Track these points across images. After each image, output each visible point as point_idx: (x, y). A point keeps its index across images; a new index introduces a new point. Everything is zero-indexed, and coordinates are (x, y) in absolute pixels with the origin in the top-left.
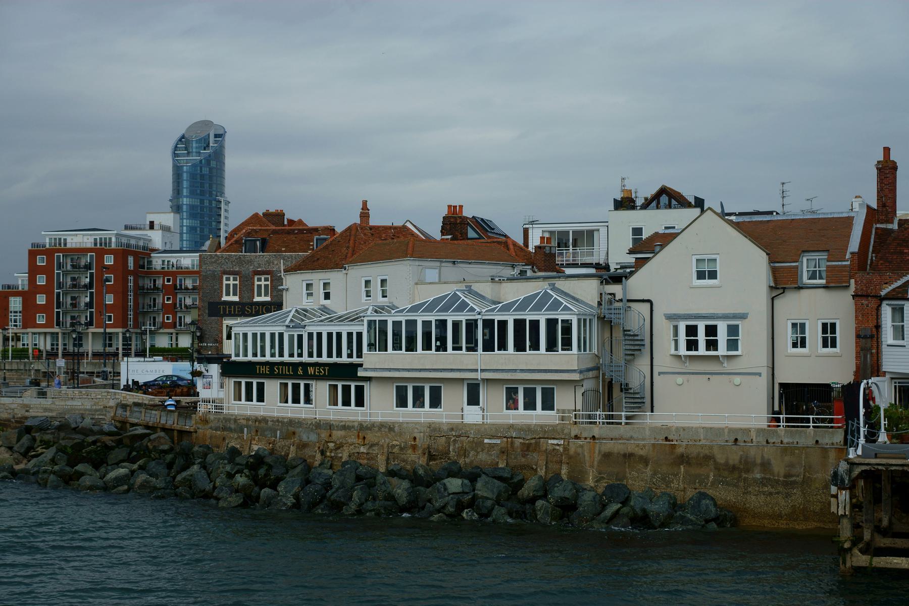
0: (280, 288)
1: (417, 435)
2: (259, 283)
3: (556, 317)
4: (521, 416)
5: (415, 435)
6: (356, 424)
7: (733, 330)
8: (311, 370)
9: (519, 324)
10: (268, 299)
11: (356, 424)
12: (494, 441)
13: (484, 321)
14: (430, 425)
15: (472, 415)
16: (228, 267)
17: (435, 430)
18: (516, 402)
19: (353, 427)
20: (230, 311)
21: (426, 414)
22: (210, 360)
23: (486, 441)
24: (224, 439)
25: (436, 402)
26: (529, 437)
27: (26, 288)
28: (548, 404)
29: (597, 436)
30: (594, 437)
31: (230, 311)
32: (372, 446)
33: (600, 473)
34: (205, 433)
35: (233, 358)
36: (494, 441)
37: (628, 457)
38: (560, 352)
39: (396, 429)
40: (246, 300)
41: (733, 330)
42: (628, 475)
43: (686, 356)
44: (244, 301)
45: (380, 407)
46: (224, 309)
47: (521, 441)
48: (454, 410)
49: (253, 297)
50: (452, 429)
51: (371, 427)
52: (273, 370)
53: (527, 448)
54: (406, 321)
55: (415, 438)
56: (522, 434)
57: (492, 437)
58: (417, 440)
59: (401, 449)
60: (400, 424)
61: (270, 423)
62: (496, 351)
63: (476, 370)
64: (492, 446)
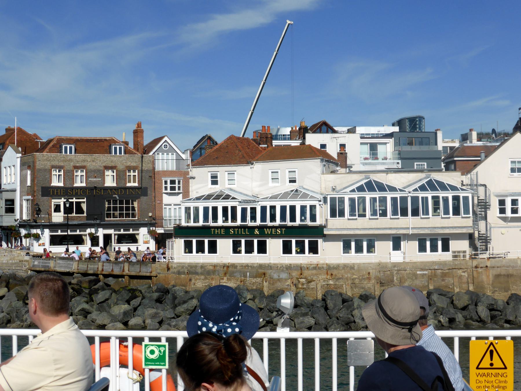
0: (188, 176)
1: (371, 271)
2: (134, 174)
3: (459, 194)
4: (429, 256)
5: (369, 271)
6: (325, 266)
7: (514, 202)
8: (267, 231)
9: (415, 200)
10: (136, 184)
11: (325, 266)
12: (425, 272)
13: (412, 197)
14: (379, 264)
15: (397, 257)
16: (56, 163)
17: (383, 267)
18: (437, 246)
19: (323, 268)
20: (57, 193)
21: (364, 258)
22: (43, 227)
23: (418, 272)
24: (190, 280)
25: (371, 248)
26: (446, 269)
27: (175, 169)
28: (446, 248)
29: (489, 266)
30: (487, 266)
31: (57, 193)
32: (339, 279)
33: (494, 288)
34: (171, 280)
35: (184, 224)
36: (425, 272)
37: (509, 276)
38: (338, 218)
39: (356, 267)
40: (68, 185)
41: (514, 202)
42: (511, 288)
43: (512, 217)
44: (67, 186)
45: (330, 253)
46: (53, 192)
47: (440, 271)
48: (384, 254)
49: (74, 184)
50: (395, 266)
51: (270, 267)
52: (226, 232)
53: (444, 275)
54: (379, 197)
55: (369, 273)
56: (441, 267)
57: (422, 270)
58: (371, 274)
59: (361, 280)
60: (359, 265)
61: (238, 267)
62: (338, 218)
63: (408, 228)
64: (423, 275)
